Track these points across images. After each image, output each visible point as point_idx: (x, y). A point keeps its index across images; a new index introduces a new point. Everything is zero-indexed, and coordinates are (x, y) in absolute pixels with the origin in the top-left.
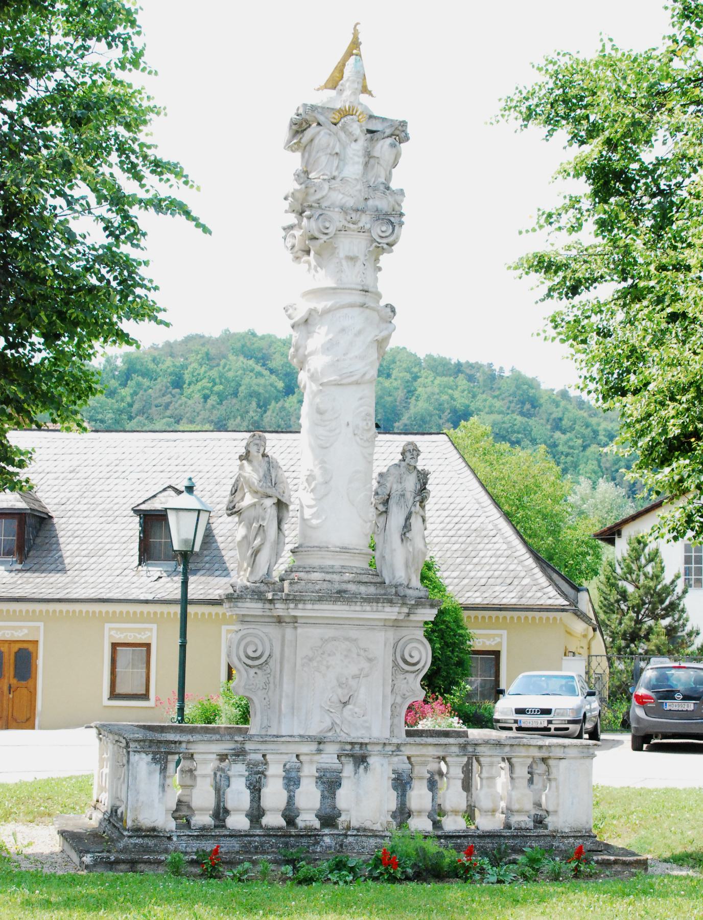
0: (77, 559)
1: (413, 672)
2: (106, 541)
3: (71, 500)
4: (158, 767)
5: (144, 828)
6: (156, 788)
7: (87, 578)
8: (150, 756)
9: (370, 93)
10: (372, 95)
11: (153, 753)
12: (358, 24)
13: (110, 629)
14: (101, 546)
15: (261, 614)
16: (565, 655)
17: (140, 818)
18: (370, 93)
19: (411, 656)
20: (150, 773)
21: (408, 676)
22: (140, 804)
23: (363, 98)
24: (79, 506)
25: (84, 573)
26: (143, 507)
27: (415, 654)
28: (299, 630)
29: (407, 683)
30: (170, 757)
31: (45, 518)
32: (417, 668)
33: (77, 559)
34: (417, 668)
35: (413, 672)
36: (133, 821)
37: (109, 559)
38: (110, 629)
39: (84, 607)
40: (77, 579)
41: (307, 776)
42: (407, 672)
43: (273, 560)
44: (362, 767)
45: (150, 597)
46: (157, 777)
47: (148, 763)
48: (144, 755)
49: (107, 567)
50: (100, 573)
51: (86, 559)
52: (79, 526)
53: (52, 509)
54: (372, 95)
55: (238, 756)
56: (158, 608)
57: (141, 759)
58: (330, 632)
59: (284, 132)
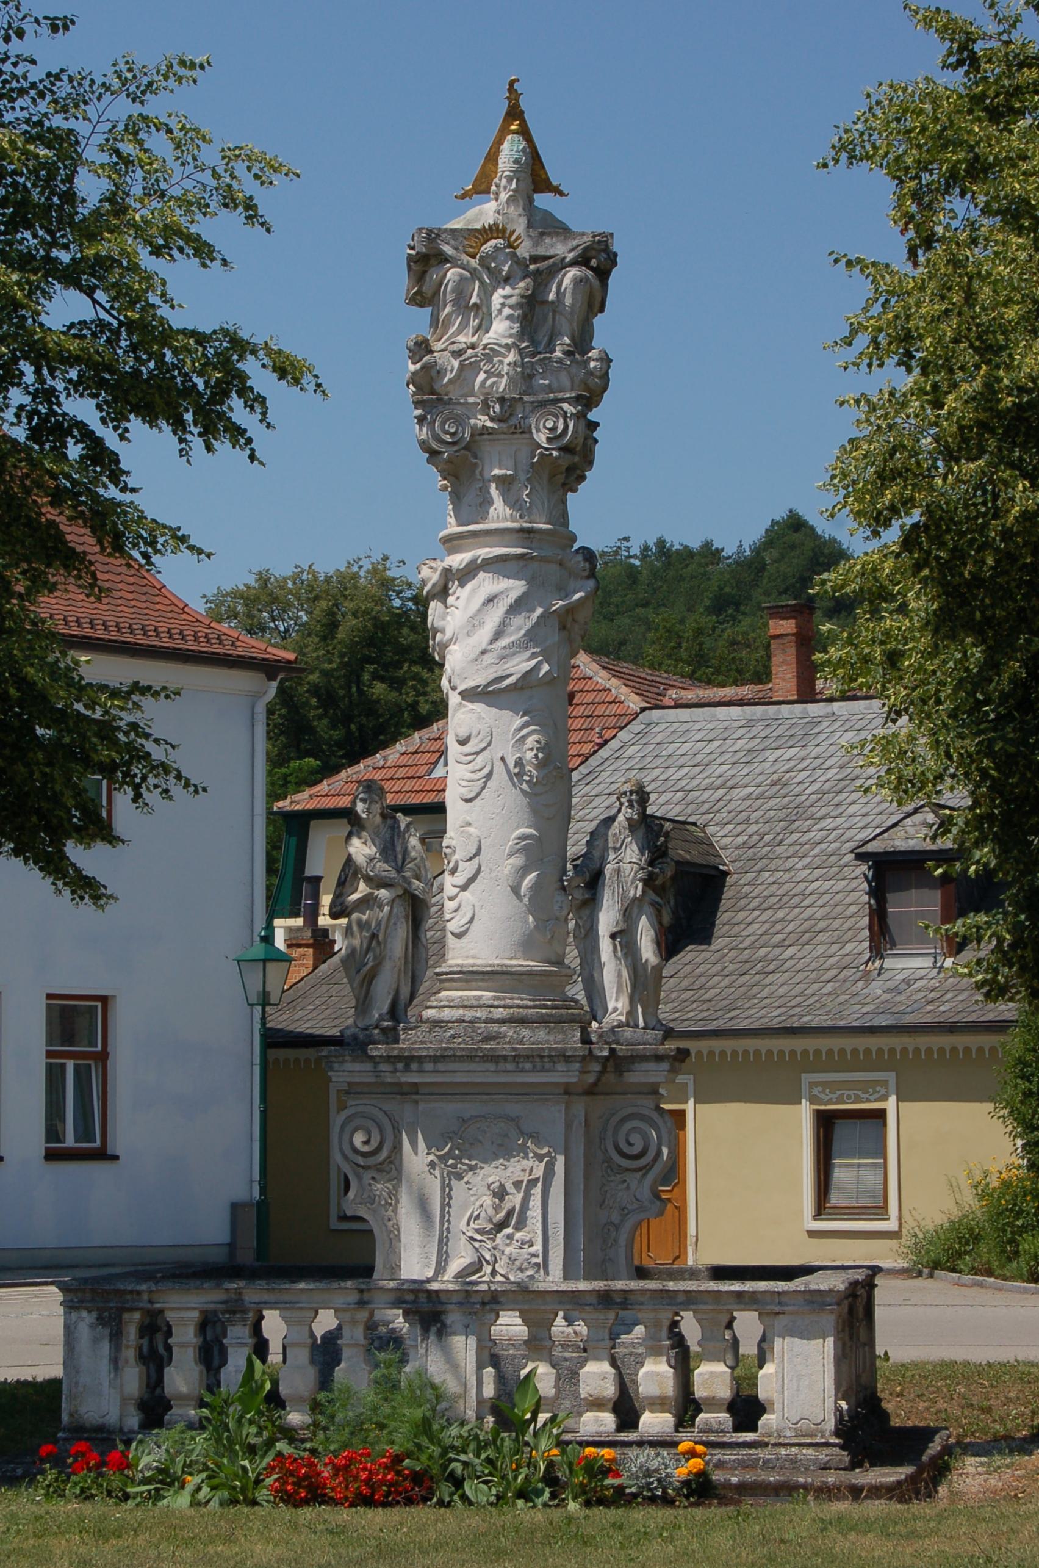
0: (762, 952)
1: (640, 1169)
2: (818, 915)
3: (767, 838)
4: (107, 1331)
5: (88, 1425)
6: (104, 1365)
7: (773, 988)
8: (94, 1314)
9: (557, 191)
10: (561, 194)
11: (98, 1309)
12: (512, 83)
13: (812, 1085)
14: (807, 924)
15: (373, 1080)
16: (102, 1155)
17: (83, 1410)
18: (557, 191)
19: (631, 1145)
20: (95, 1341)
21: (628, 1176)
22: (81, 1389)
23: (543, 201)
24: (779, 850)
25: (771, 978)
26: (870, 848)
27: (636, 1138)
28: (422, 1106)
29: (628, 1188)
30: (126, 1316)
31: (713, 876)
32: (642, 1162)
33: (762, 952)
34: (642, 1162)
35: (640, 1169)
36: (71, 1415)
37: (820, 949)
38: (812, 1085)
39: (763, 1044)
40: (755, 990)
41: (348, 1345)
42: (627, 1170)
43: (405, 991)
44: (434, 1329)
45: (883, 1021)
46: (105, 1347)
47: (92, 1326)
48: (84, 1314)
49: (814, 965)
50: (801, 976)
51: (777, 951)
52: (774, 888)
53: (727, 858)
54: (561, 194)
55: (234, 1312)
56: (897, 1042)
57: (83, 1319)
58: (470, 1108)
59: (401, 281)
